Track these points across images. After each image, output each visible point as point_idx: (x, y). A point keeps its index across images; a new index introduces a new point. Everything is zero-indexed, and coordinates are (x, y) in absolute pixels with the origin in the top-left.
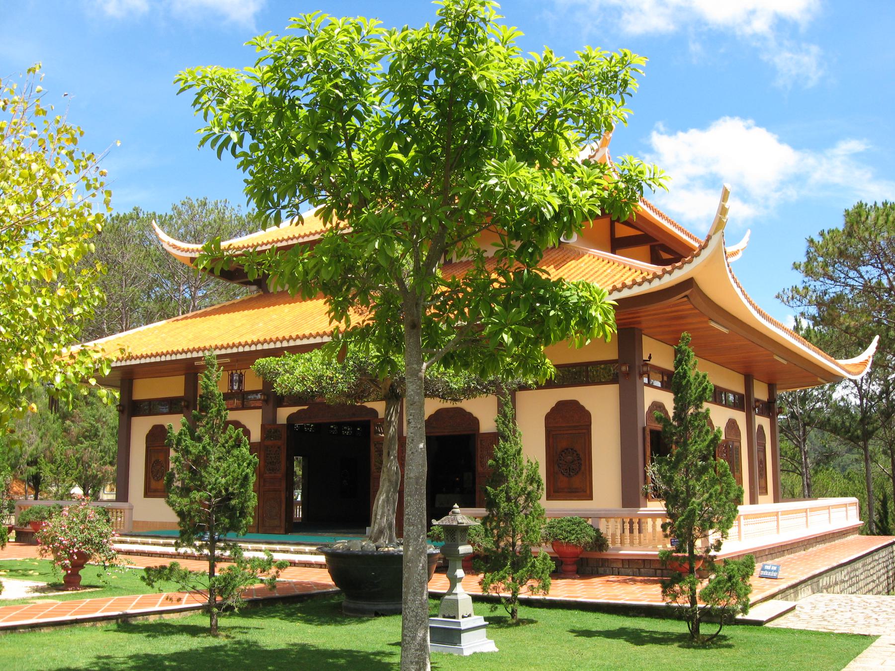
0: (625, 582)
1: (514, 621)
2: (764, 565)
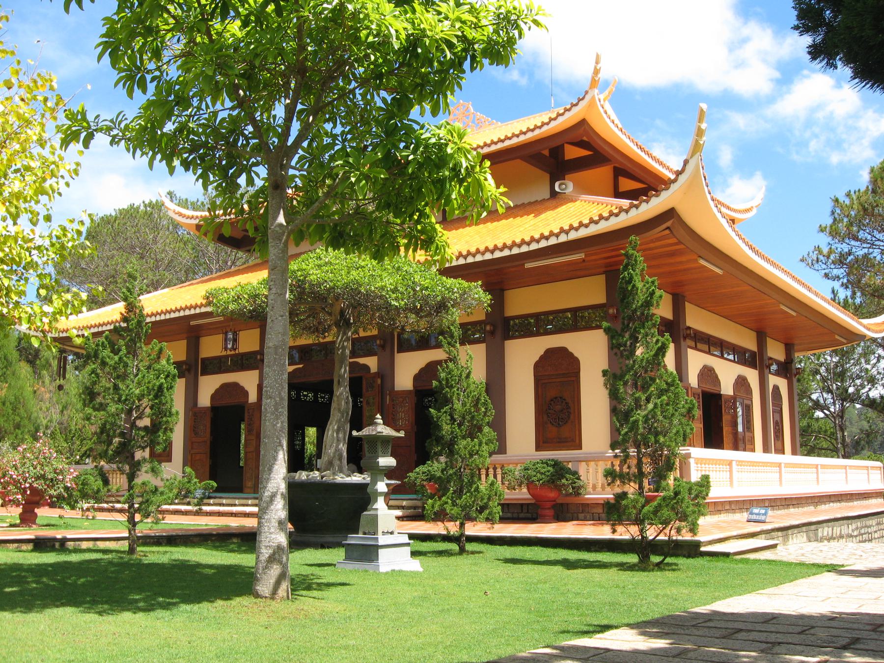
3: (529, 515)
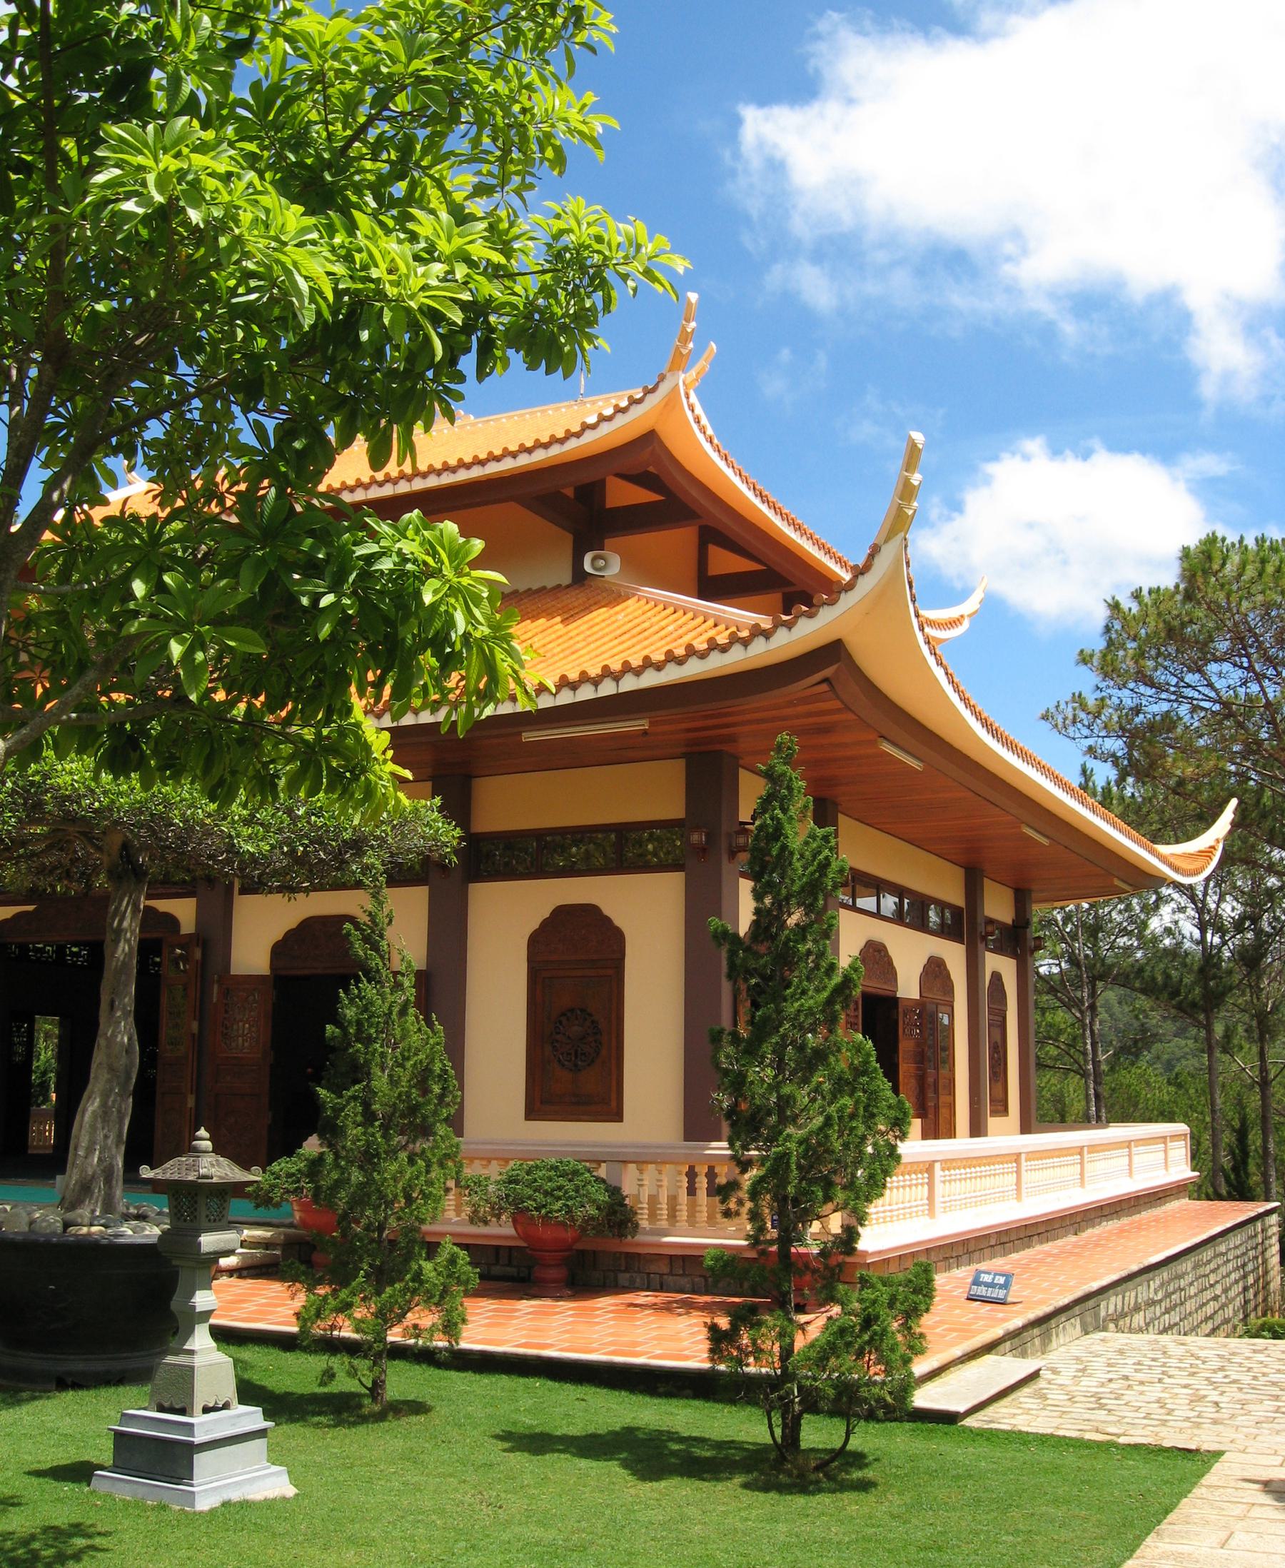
0: (667, 1308)
1: (377, 1408)
2: (979, 1272)
3: (511, 1271)
